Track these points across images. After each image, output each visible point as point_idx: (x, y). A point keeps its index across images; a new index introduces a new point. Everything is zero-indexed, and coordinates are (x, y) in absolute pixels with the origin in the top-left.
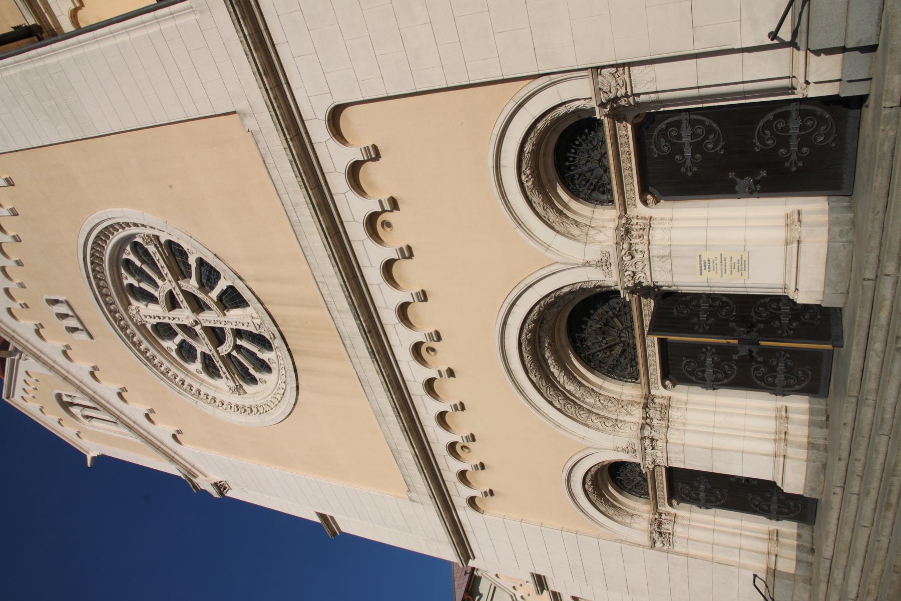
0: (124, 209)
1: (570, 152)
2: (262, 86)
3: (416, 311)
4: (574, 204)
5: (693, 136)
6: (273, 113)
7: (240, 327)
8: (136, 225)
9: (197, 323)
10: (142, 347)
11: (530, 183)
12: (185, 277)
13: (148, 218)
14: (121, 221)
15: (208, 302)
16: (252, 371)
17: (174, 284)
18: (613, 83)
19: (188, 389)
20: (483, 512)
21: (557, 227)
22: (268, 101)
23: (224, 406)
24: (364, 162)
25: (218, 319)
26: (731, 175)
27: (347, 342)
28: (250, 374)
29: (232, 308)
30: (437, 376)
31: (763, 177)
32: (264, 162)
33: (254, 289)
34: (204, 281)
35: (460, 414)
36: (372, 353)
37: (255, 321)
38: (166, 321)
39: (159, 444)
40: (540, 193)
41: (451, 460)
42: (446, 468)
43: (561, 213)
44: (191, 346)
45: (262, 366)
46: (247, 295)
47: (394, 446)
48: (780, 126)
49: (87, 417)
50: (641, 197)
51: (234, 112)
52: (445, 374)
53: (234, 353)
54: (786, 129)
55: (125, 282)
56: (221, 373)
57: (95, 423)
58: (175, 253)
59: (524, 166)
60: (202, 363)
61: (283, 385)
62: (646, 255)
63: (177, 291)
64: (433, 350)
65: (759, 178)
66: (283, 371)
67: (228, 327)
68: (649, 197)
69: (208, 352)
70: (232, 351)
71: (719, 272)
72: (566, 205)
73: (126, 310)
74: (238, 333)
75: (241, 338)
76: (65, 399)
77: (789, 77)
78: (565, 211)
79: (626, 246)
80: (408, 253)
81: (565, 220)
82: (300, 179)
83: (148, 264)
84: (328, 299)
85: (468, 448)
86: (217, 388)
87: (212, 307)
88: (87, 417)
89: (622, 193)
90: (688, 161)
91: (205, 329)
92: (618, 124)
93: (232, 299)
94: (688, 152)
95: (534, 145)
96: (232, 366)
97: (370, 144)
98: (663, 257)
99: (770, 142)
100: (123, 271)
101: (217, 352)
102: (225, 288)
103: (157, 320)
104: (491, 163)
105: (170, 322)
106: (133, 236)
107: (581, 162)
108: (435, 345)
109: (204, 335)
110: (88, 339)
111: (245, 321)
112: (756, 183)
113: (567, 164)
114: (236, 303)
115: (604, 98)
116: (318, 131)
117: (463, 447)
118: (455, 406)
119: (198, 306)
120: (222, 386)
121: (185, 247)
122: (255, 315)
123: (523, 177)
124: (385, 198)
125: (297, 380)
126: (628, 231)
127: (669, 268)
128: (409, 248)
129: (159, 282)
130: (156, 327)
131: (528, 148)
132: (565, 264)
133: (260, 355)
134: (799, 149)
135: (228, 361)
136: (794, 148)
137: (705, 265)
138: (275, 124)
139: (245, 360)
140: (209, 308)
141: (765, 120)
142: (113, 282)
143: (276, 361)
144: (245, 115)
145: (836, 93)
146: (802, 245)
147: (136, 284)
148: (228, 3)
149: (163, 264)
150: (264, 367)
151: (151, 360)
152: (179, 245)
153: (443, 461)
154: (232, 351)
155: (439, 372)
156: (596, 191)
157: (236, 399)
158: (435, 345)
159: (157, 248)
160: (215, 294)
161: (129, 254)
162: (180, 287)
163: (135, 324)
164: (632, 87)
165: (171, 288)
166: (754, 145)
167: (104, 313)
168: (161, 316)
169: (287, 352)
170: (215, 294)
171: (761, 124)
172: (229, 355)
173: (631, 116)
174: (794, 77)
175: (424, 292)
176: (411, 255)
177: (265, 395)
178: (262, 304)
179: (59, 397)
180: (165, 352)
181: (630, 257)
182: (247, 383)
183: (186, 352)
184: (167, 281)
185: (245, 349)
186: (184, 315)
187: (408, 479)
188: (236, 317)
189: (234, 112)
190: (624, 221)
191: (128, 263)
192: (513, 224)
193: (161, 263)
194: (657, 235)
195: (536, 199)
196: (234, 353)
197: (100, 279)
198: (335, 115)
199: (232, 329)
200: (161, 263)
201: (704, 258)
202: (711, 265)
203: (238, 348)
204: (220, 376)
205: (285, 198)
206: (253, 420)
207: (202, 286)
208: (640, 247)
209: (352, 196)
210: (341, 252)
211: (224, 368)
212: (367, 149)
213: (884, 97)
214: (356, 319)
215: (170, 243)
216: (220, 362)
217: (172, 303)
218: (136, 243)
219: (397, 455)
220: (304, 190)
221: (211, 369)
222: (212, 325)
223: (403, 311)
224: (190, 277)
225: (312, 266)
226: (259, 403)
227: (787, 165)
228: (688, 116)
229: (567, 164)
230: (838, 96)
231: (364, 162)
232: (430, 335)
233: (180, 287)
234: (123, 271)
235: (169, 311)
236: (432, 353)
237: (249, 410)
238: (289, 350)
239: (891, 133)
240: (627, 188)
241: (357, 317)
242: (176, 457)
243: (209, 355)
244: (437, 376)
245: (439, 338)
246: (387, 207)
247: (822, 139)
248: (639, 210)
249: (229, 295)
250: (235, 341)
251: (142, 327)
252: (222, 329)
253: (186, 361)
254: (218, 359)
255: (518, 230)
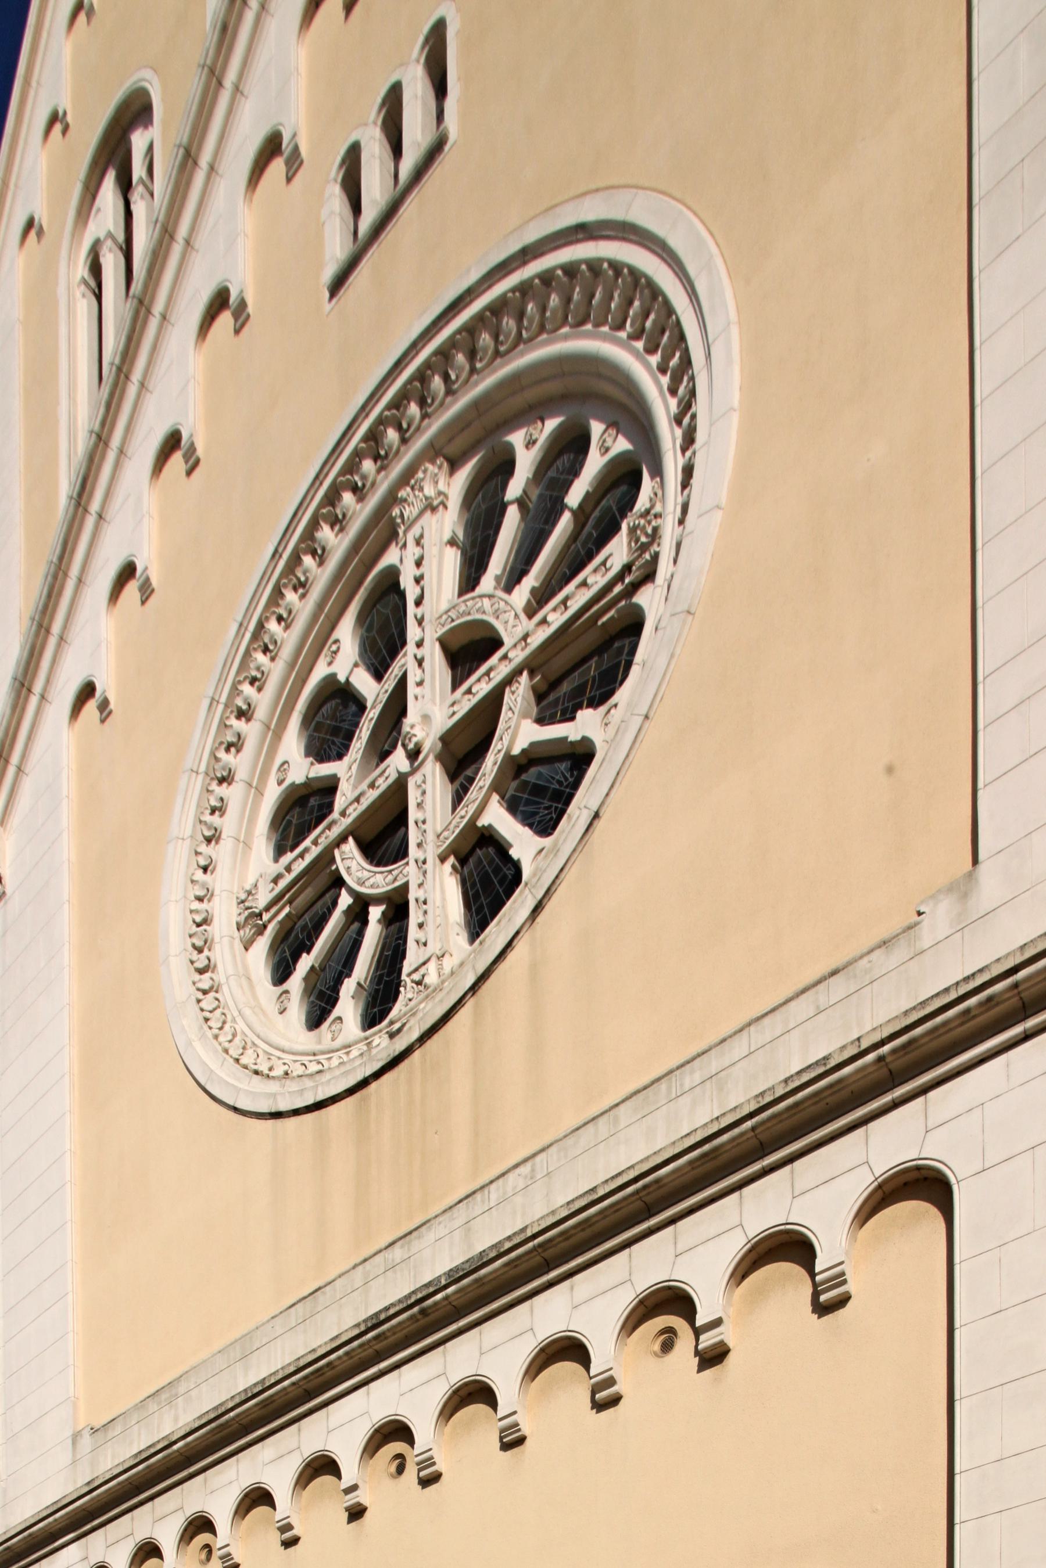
0: (735, 418)
2: (1029, 954)
3: (479, 1425)
6: (953, 995)
7: (414, 916)
8: (688, 472)
9: (414, 755)
10: (326, 534)
12: (540, 696)
13: (706, 531)
14: (700, 406)
15: (475, 794)
16: (305, 963)
17: (518, 656)
19: (230, 738)
20: (852, 1236)
22: (985, 977)
23: (199, 875)
24: (812, 1274)
25: (430, 837)
27: (397, 1253)
28: (296, 958)
29: (463, 882)
30: (347, 1481)
32: (834, 973)
33: (512, 956)
34: (531, 775)
35: (275, 1538)
36: (375, 1322)
37: (432, 966)
38: (413, 632)
39: (56, 628)
41: (293, 1465)
42: (158, 1514)
44: (349, 736)
45: (321, 995)
46: (497, 934)
47: (182, 1388)
49: (96, 269)
51: (975, 861)
52: (351, 1499)
53: (345, 900)
55: (517, 439)
56: (289, 856)
57: (84, 305)
58: (593, 661)
60: (309, 783)
61: (278, 1072)
63: (497, 668)
64: (401, 1470)
66: (313, 1068)
67: (408, 872)
69: (340, 802)
70: (351, 892)
73: (432, 452)
74: (398, 909)
75: (387, 920)
76: (139, 141)
80: (605, 1399)
82: (780, 1092)
83: (574, 537)
84: (494, 1193)
85: (208, 1559)
86: (247, 845)
87: (461, 811)
88: (96, 269)
91: (400, 787)
93: (486, 881)
96: (309, 894)
97: (851, 1287)
100: (552, 424)
101: (342, 839)
102: (514, 853)
103: (411, 593)
105: (410, 648)
106: (657, 471)
108: (411, 1473)
109: (383, 785)
110: (329, 273)
111: (430, 933)
114: (476, 896)
116: (891, 1141)
117: (208, 1548)
118: (289, 1527)
119: (463, 751)
120: (253, 867)
121: (623, 695)
122: (448, 964)
124: (726, 1334)
125: (296, 1112)
128: (615, 1401)
129: (521, 594)
130: (390, 587)
133: (348, 987)
135: (322, 880)
138: (923, 1004)
139: (328, 942)
140: (458, 799)
142: (514, 383)
143: (338, 1043)
144: (965, 896)
147: (515, 489)
148: (1040, 948)
149: (575, 606)
150: (320, 1008)
151: (292, 576)
152: (629, 665)
153: (172, 1506)
154: (351, 892)
155: (354, 1488)
157: (225, 915)
158: (411, 1473)
159: (620, 577)
160: (498, 818)
161: (606, 446)
162: (509, 680)
163: (392, 499)
165: (508, 641)
167: (415, 347)
168: (426, 608)
169: (359, 1077)
170: (498, 818)
172: (338, 882)
175: (521, 1441)
176: (599, 1406)
177: (247, 1012)
178: (474, 988)
179: (135, 111)
180: (321, 640)
182: (275, 947)
183: (332, 720)
184: (527, 624)
185: (361, 933)
186: (435, 707)
187: (118, 1428)
188: (439, 894)
189: (975, 861)
191: (571, 446)
193: (577, 596)
196: (345, 900)
197: (521, 315)
198: (925, 1185)
199: (405, 887)
200: (577, 596)
203: (359, 913)
204: (280, 851)
205: (739, 1048)
206: (178, 979)
207: (518, 766)
209: (734, 1247)
210: (935, 1044)
211: (299, 866)
212: (840, 1279)
214: (449, 1274)
215: (632, 626)
216: (315, 851)
217: (469, 650)
218: (635, 482)
219: (164, 1396)
220: (753, 1106)
221: (294, 818)
222: (413, 814)
223: (569, 1349)
224: (541, 721)
225: (570, 1141)
226: (225, 995)
231: (812, 1274)
232: (430, 1462)
233: (509, 680)
234: (552, 424)
235: (443, 642)
236: (393, 1468)
237: (201, 962)
238: (364, 1083)
241: (455, 1276)
242: (34, 700)
243: (329, 807)
244: (347, 1481)
245: (426, 1482)
246: (707, 1340)
249: (497, 870)
250: (377, 900)
251: (384, 529)
252: (402, 853)
253: (307, 720)
254: (323, 842)
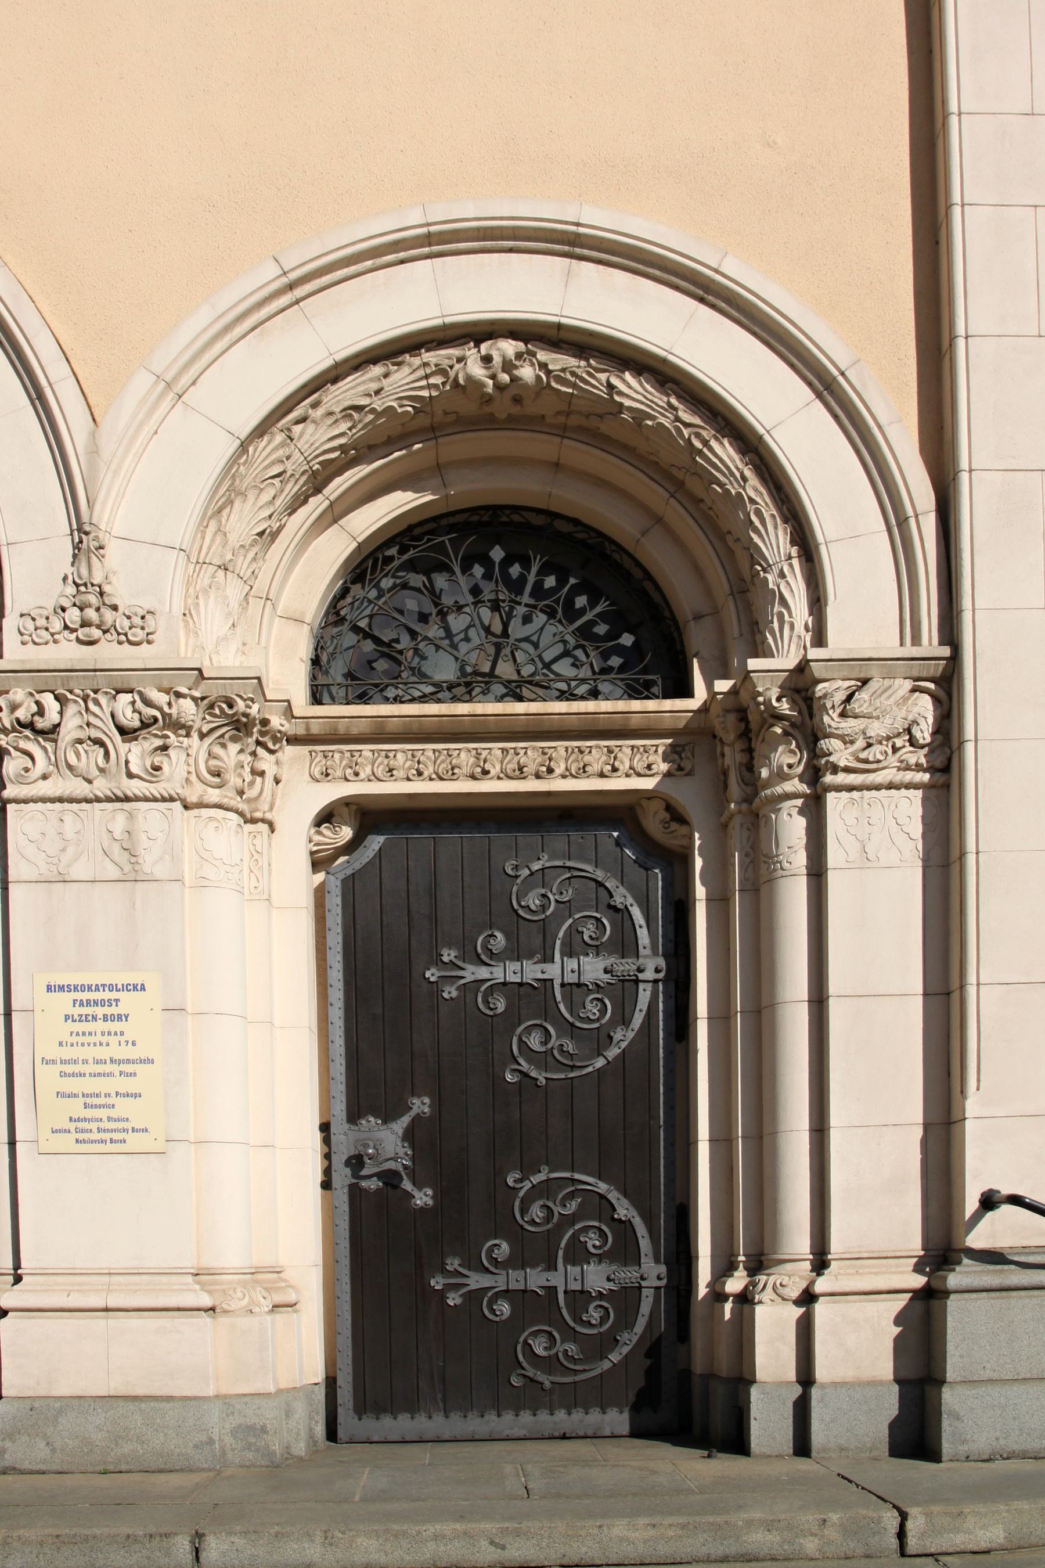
1: (543, 572)
4: (335, 549)
5: (575, 989)
11: (477, 371)
18: (877, 729)
21: (266, 449)
26: (421, 1105)
31: (410, 1196)
40: (424, 406)
43: (317, 483)
48: (592, 1241)
50: (347, 802)
54: (578, 1254)
59: (558, 361)
62: (135, 787)
65: (407, 1185)
68: (346, 833)
71: (67, 1053)
72: (334, 515)
77: (17, 1265)
78: (317, 505)
79: (187, 709)
81: (291, 489)
89: (380, 734)
90: (483, 973)
92: (663, 743)
94: (511, 972)
95: (639, 416)
98: (131, 852)
99: (536, 1212)
104: (598, 217)
107: (467, 610)
112: (390, 1179)
113: (497, 554)
115: (832, 690)
123: (509, 347)
126: (241, 726)
127: (79, 871)
131: (634, 391)
132: (94, 450)
134: (506, 1294)
136: (499, 1281)
137: (96, 1004)
141: (614, 1196)
145: (760, 1375)
146: (205, 1319)
156: (367, 642)
164: (851, 788)
166: (527, 1170)
171: (602, 1187)
173: (689, 796)
174: (18, 1279)
181: (131, 720)
190: (277, 722)
192: (303, 253)
194: (222, 836)
195: (401, 383)
201: (128, 1002)
202: (100, 1026)
208: (177, 768)
213: (936, 1509)
227: (453, 1263)
228: (649, 975)
229: (497, 554)
230: (753, 1381)
239: (811, 1546)
240: (401, 754)
247: (540, 1351)
248: (302, 791)
255: (267, 275)
